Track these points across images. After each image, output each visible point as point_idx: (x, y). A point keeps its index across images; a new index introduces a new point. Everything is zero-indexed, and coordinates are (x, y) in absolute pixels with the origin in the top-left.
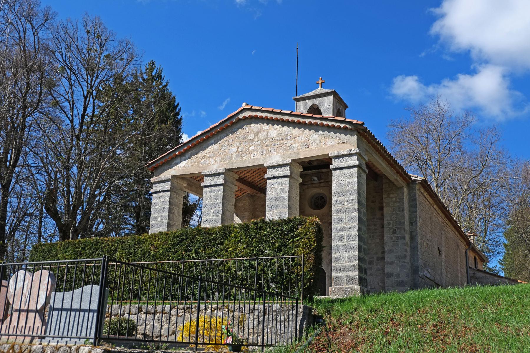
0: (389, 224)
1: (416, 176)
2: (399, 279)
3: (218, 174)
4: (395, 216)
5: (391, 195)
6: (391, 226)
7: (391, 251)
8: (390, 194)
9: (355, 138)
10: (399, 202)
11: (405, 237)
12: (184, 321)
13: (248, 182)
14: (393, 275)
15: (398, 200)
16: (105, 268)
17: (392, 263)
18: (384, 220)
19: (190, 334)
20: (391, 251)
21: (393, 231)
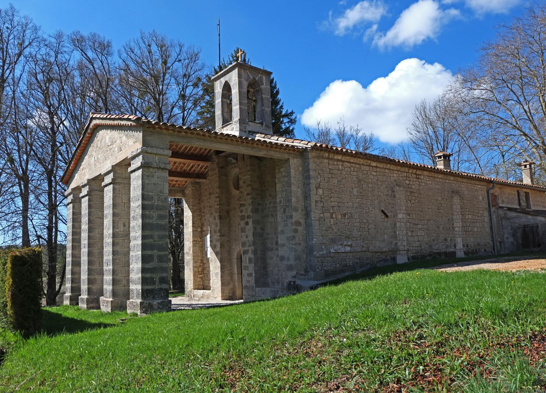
0: (280, 202)
1: (307, 143)
2: (289, 263)
3: (137, 155)
4: (285, 193)
5: (282, 170)
6: (282, 204)
7: (283, 232)
8: (280, 168)
9: (141, 134)
10: (287, 176)
11: (292, 215)
12: (104, 68)
13: (173, 172)
14: (284, 259)
15: (286, 174)
16: (108, 222)
17: (283, 245)
18: (277, 198)
19: (104, 68)
20: (283, 232)
21: (284, 211)
